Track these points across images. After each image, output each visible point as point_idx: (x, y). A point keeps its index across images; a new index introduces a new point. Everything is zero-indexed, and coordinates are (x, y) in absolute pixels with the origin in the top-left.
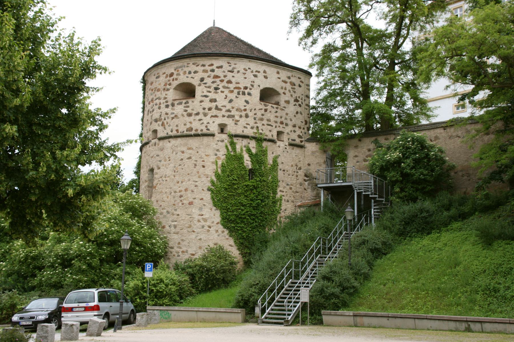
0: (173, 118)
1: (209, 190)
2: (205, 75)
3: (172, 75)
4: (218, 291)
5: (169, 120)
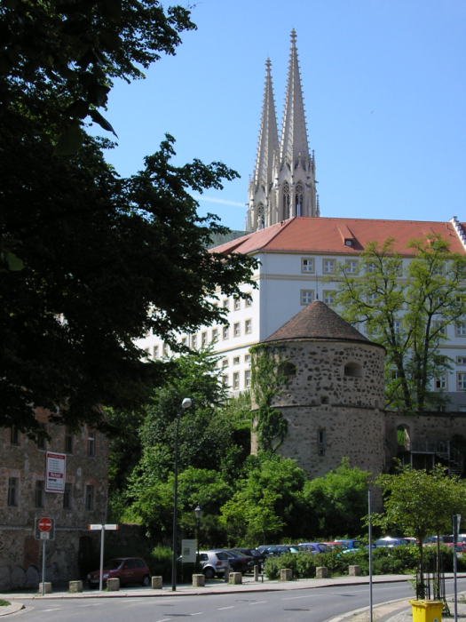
2: (367, 359)
3: (341, 353)
5: (342, 392)
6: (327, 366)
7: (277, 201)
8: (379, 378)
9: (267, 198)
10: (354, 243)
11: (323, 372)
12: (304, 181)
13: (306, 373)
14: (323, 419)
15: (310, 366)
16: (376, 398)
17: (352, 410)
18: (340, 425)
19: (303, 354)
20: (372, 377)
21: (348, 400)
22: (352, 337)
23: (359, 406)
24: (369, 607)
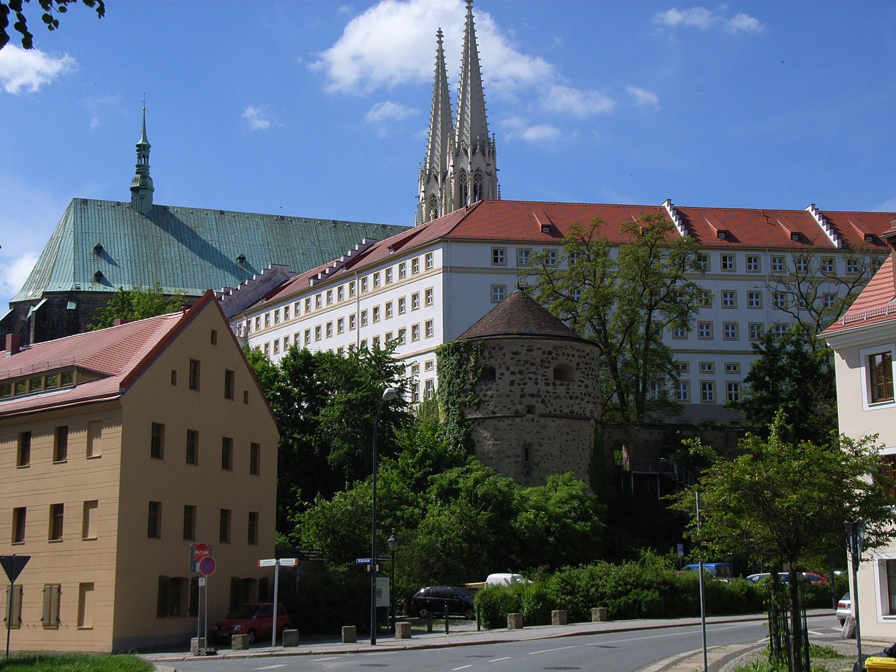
0: (555, 398)
1: (588, 472)
2: (580, 360)
3: (550, 353)
4: (21, 652)
5: (551, 399)
6: (533, 369)
7: (453, 186)
8: (594, 382)
9: (470, 163)
10: (552, 230)
11: (528, 376)
12: (483, 168)
13: (508, 377)
14: (529, 433)
15: (512, 369)
16: (591, 406)
17: (563, 421)
18: (549, 439)
19: (504, 355)
20: (586, 382)
21: (558, 409)
22: (561, 333)
23: (572, 416)
24: (703, 649)
